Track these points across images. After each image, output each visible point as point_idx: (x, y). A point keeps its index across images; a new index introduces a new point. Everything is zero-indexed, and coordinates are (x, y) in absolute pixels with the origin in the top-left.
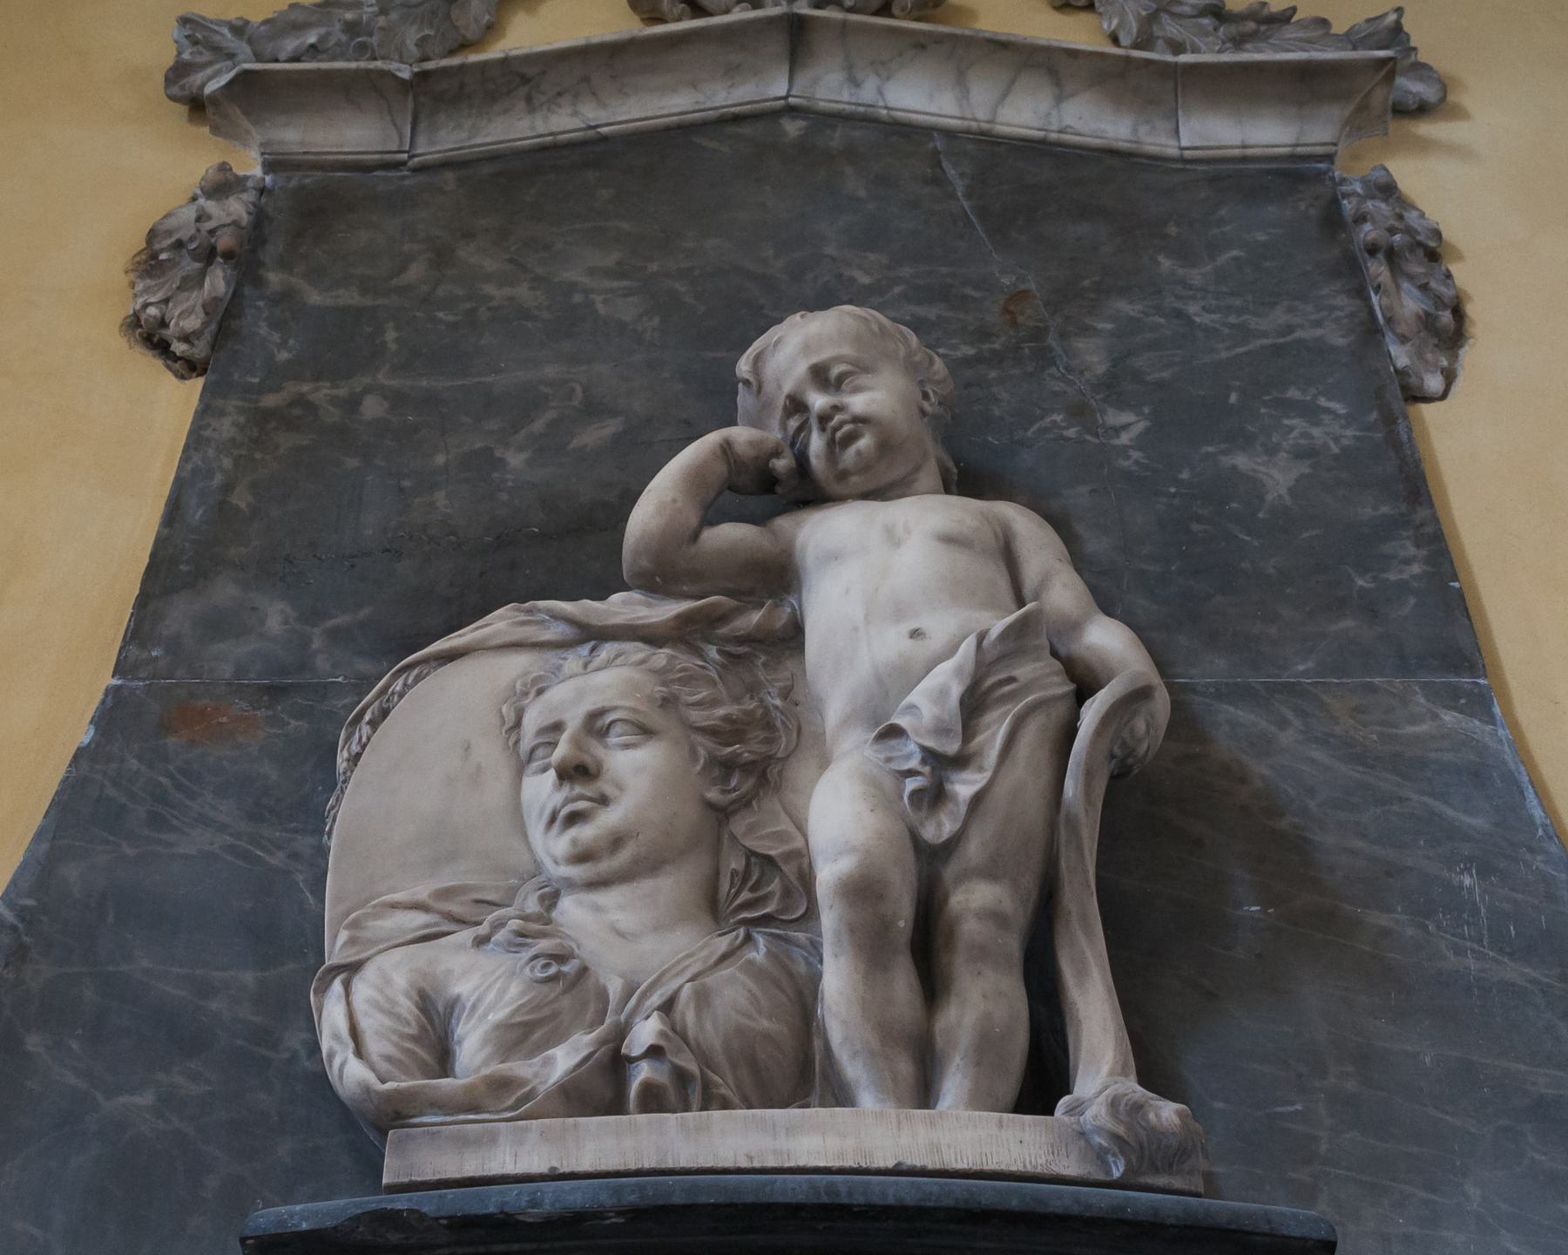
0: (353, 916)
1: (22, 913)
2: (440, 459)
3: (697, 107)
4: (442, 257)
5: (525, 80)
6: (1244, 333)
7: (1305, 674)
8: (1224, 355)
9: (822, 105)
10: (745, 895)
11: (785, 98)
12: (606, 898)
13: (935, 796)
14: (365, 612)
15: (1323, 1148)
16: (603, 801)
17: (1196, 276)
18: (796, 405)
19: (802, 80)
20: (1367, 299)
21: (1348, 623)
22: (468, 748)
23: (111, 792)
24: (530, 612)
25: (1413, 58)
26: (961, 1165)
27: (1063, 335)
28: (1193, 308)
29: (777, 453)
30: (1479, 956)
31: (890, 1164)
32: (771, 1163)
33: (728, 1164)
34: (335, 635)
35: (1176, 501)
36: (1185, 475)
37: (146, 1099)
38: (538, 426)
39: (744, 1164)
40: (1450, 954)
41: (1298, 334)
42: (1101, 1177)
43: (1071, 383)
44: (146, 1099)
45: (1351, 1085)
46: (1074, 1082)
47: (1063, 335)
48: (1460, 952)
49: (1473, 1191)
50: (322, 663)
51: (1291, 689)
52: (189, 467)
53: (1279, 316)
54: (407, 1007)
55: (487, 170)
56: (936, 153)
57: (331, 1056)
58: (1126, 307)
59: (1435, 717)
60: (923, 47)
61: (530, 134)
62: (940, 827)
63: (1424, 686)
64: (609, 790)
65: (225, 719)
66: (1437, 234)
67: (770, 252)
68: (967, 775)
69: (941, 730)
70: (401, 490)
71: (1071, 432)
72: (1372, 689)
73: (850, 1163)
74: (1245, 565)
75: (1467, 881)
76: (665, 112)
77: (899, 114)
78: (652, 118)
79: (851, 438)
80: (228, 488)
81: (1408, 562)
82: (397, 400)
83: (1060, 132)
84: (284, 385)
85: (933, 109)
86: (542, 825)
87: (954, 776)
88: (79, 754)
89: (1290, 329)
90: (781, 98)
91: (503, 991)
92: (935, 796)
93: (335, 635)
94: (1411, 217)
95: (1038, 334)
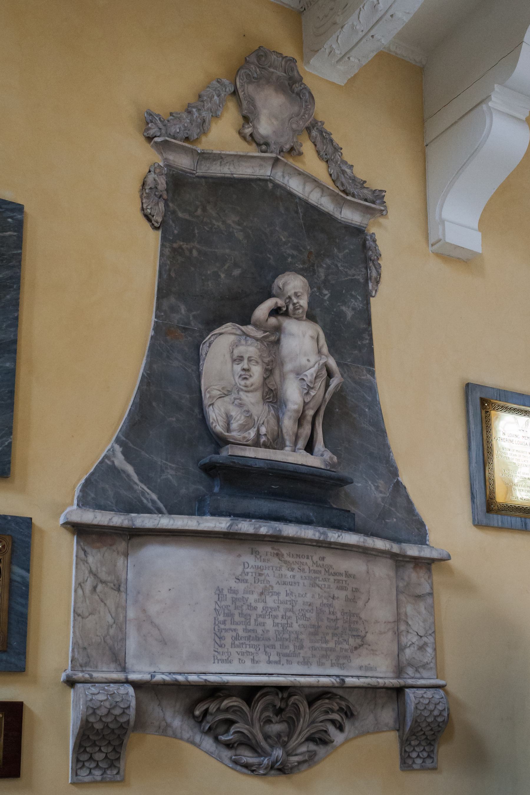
0: (208, 390)
1: (147, 374)
2: (209, 272)
3: (253, 174)
4: (204, 210)
5: (222, 158)
6: (347, 275)
7: (349, 362)
8: (343, 279)
9: (277, 181)
10: (268, 397)
11: (270, 176)
12: (249, 395)
13: (308, 393)
14: (199, 312)
15: (343, 456)
16: (251, 376)
17: (341, 255)
18: (290, 298)
19: (274, 171)
20: (367, 270)
21: (356, 352)
22: (224, 356)
23: (159, 348)
24: (234, 326)
25: (385, 204)
26: (310, 465)
27: (317, 267)
28: (339, 265)
29: (284, 307)
30: (367, 425)
31: (300, 463)
32: (285, 461)
33: (279, 460)
34: (194, 316)
35: (333, 316)
36: (335, 310)
37: (174, 419)
38: (226, 267)
39: (282, 461)
40: (363, 424)
41: (356, 277)
42: (326, 468)
43: (318, 280)
44: (174, 419)
45: (347, 446)
46: (315, 444)
47: (317, 267)
48: (364, 424)
49: (361, 467)
50: (192, 323)
51: (346, 364)
52: (161, 262)
53: (352, 272)
54: (224, 416)
55: (210, 180)
56: (297, 203)
57: (212, 423)
58: (328, 261)
59: (366, 375)
60: (300, 174)
61: (219, 172)
62: (307, 399)
63: (366, 368)
64: (252, 375)
65: (177, 334)
66: (381, 255)
67: (266, 226)
68: (313, 390)
69: (311, 382)
70: (202, 279)
71: (318, 294)
72: (358, 367)
73: (295, 462)
74: (342, 335)
75: (367, 410)
76: (246, 173)
77: (291, 189)
78: (244, 175)
79: (298, 309)
80: (170, 270)
81: (366, 339)
82: (199, 251)
83: (320, 205)
84: (177, 241)
85: (297, 190)
86: (238, 377)
87: (311, 390)
88: (152, 337)
89: (354, 275)
90: (268, 176)
91: (240, 417)
92: (308, 393)
93: (194, 316)
94: (377, 248)
95: (313, 265)
